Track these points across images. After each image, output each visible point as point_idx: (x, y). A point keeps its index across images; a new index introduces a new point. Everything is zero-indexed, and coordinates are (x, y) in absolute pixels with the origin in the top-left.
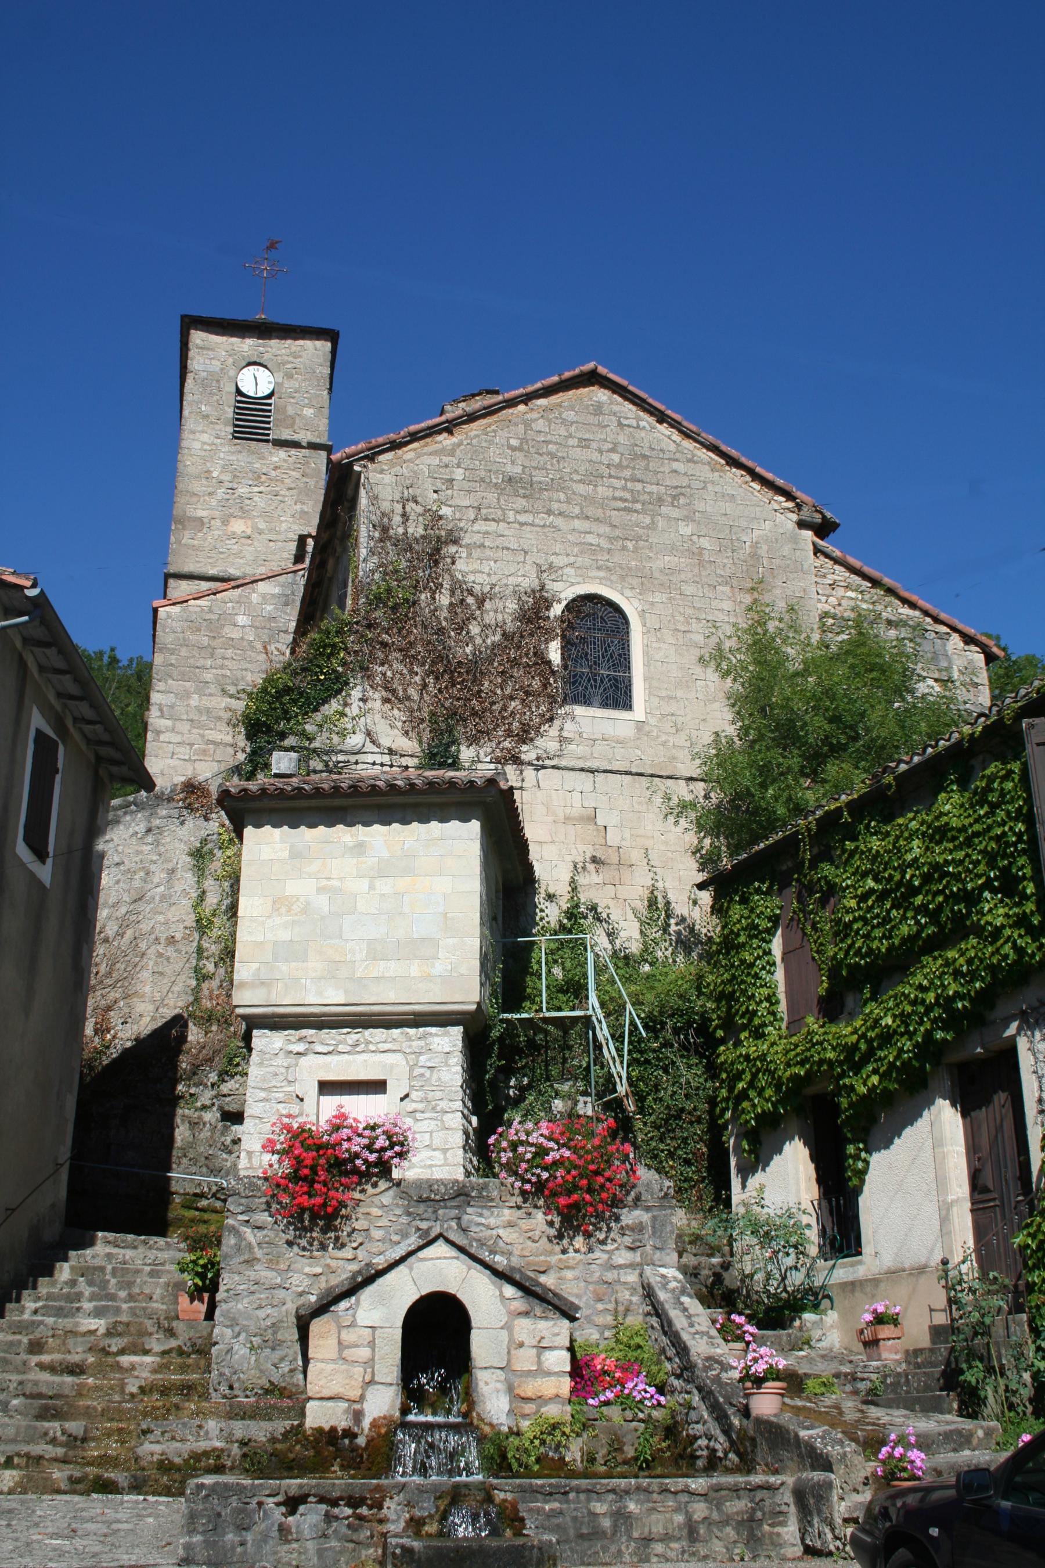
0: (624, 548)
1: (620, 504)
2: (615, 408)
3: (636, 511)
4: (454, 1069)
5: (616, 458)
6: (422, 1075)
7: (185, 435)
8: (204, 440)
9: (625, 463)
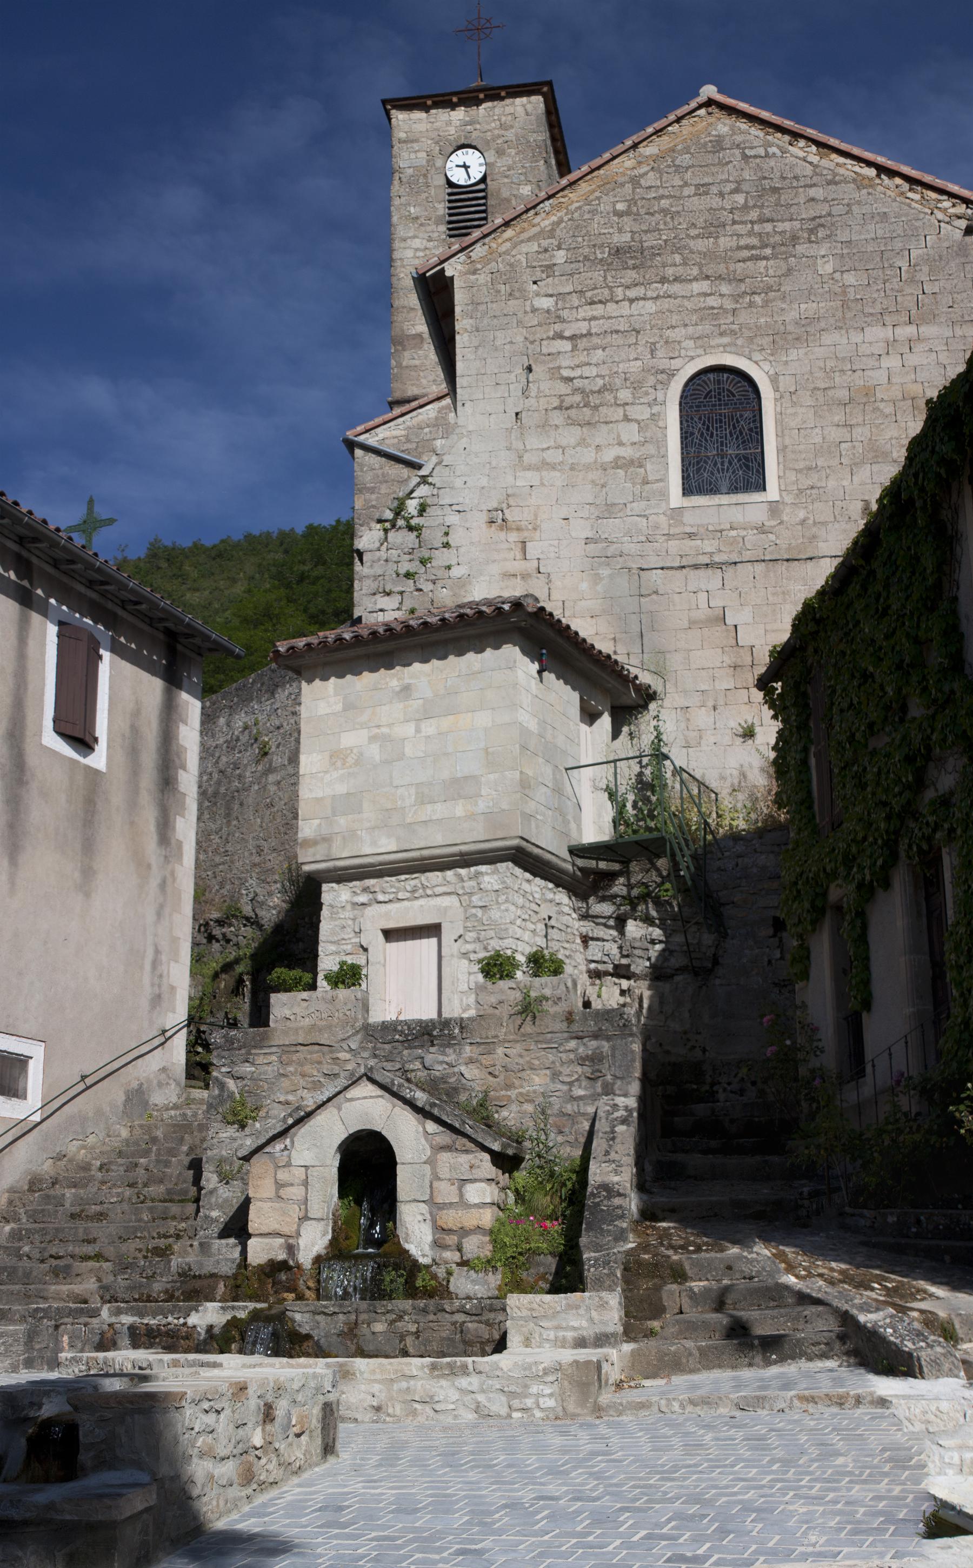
0: (751, 304)
1: (746, 254)
3: (766, 258)
5: (740, 199)
7: (397, 244)
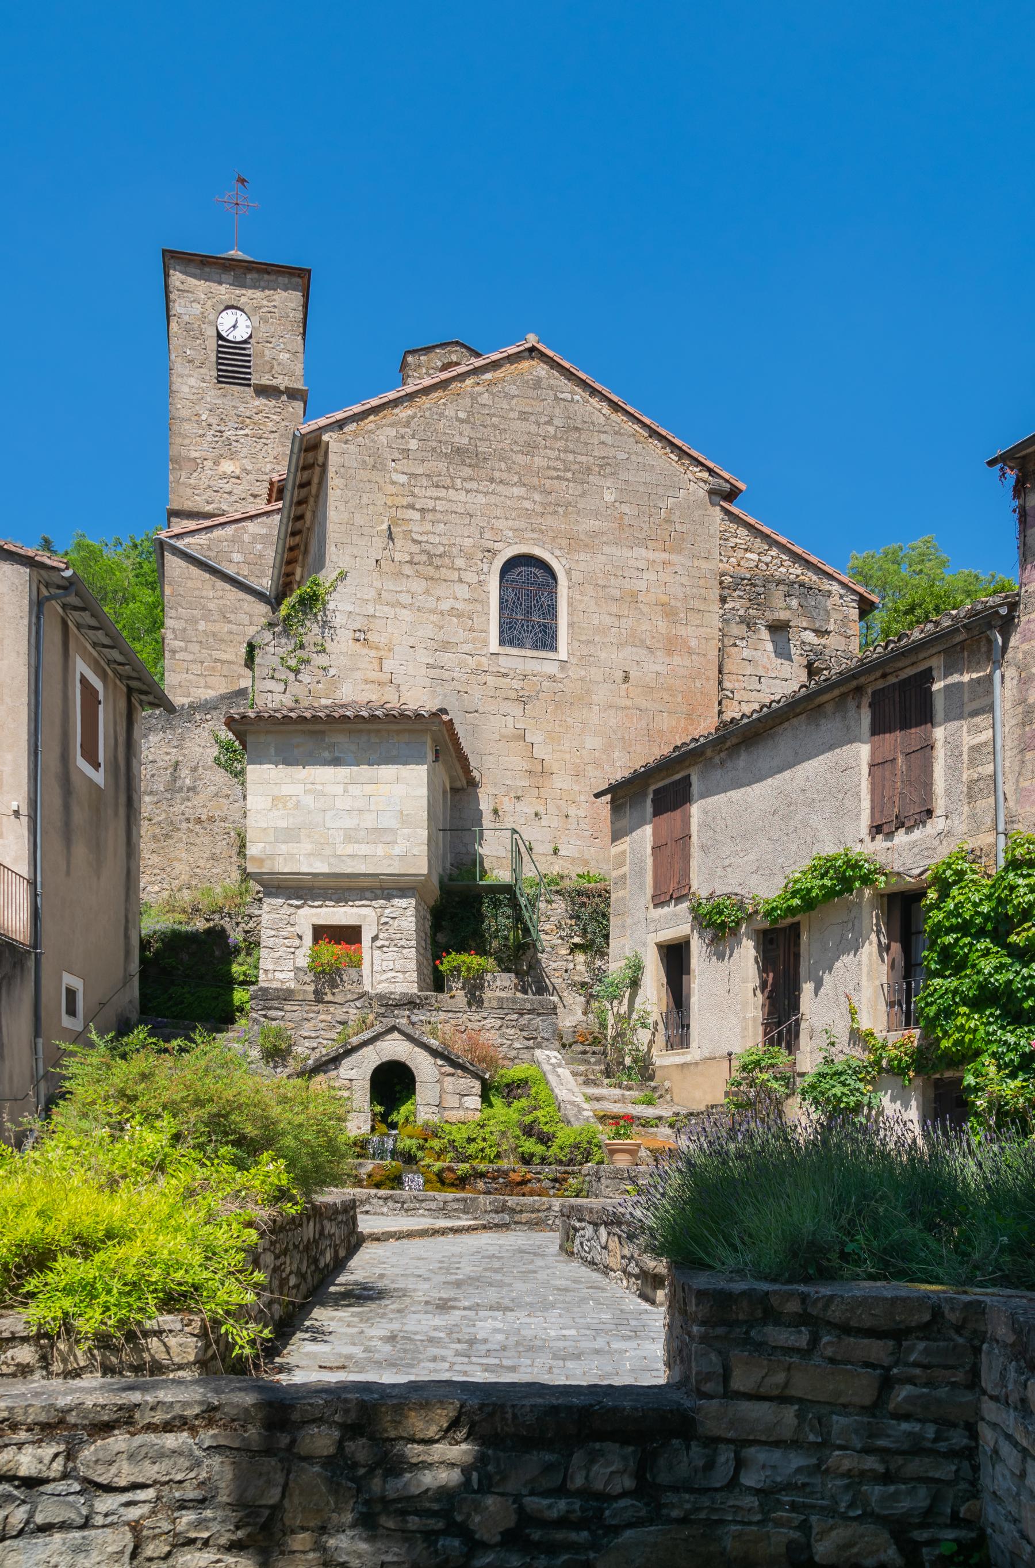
2: (553, 382)
6: (386, 923)
8: (192, 383)
9: (559, 435)
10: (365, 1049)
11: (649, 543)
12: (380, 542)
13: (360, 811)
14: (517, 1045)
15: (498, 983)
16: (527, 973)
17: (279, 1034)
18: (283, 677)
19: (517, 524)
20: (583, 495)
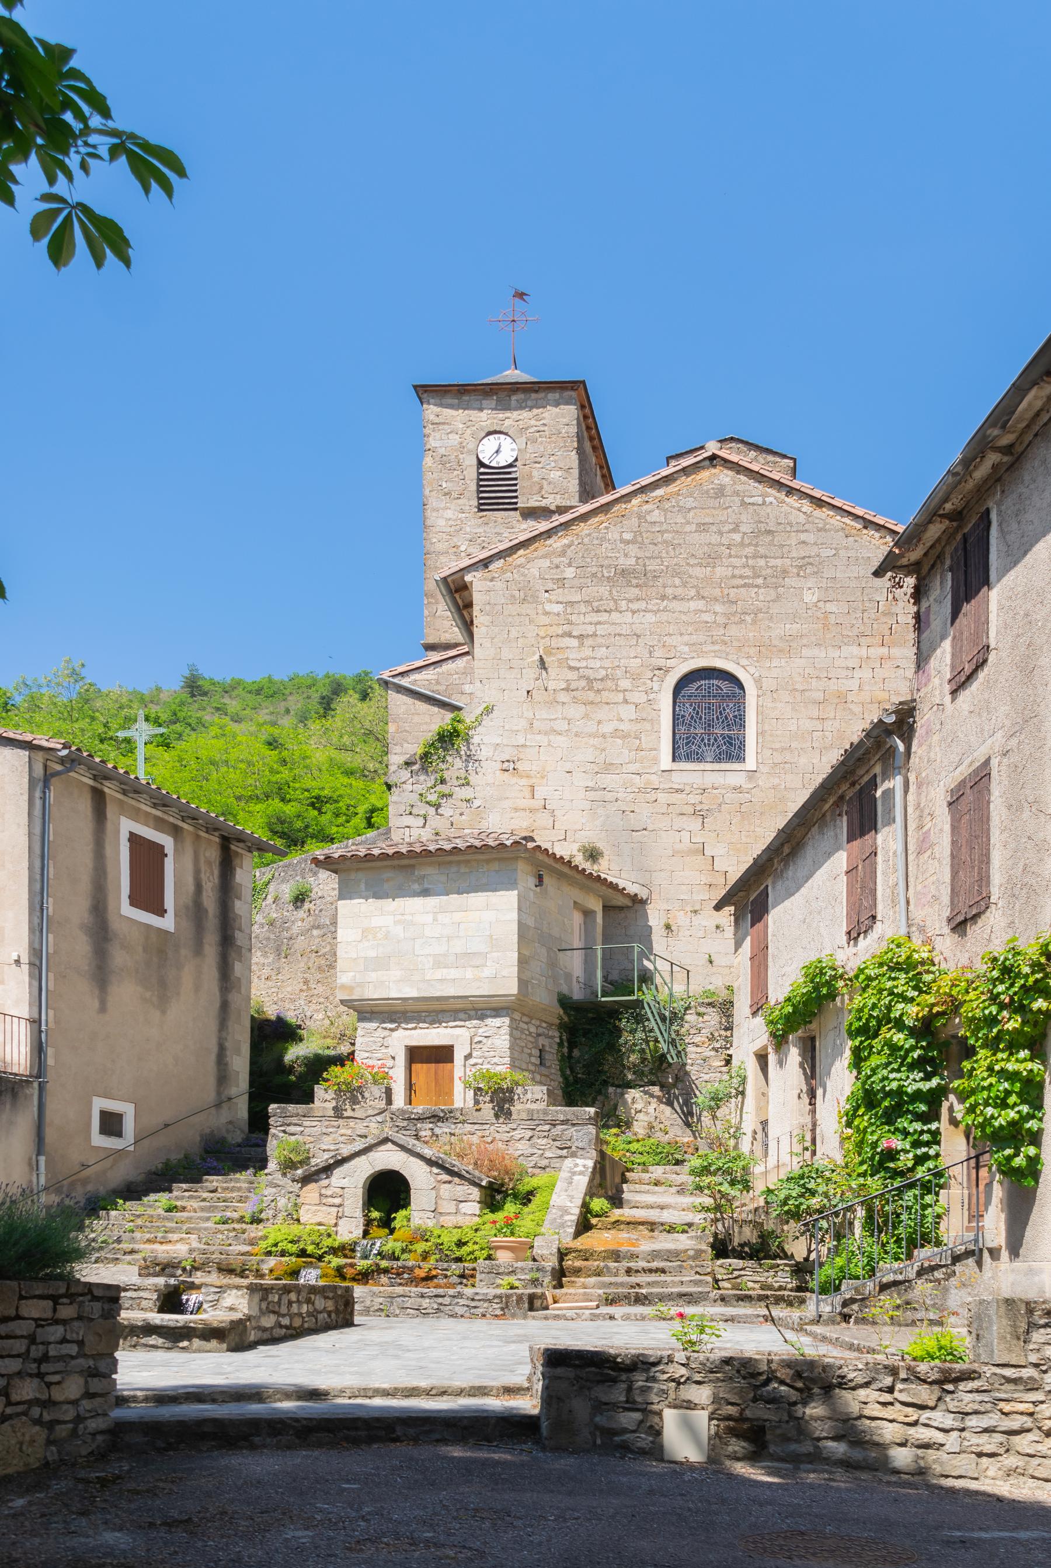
1: (741, 582)
2: (738, 487)
4: (503, 1037)
6: (480, 1042)
9: (747, 541)
10: (357, 1159)
11: (863, 640)
12: (532, 673)
13: (449, 938)
14: (548, 1154)
15: (529, 1096)
16: (674, 1085)
17: (295, 1150)
18: (422, 812)
19: (694, 638)
20: (778, 598)
